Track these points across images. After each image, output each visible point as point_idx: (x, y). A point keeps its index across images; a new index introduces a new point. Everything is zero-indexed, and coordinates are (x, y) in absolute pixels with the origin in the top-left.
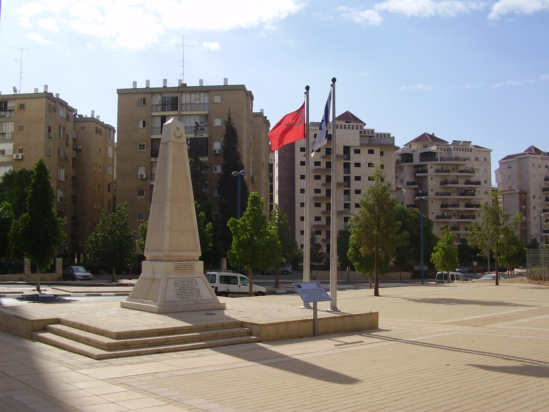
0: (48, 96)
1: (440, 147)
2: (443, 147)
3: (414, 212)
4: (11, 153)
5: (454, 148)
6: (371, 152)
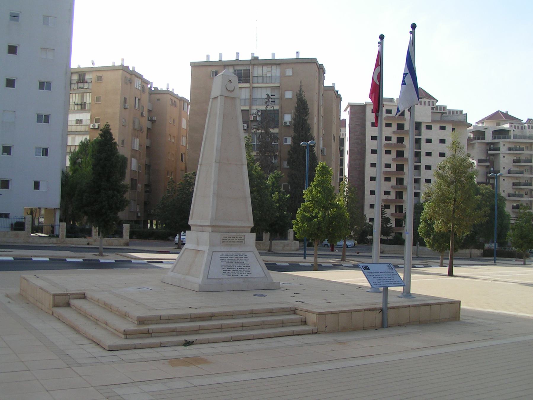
0: (125, 69)
1: (513, 125)
2: (517, 125)
3: (487, 189)
4: (88, 123)
5: (529, 126)
6: (443, 128)
